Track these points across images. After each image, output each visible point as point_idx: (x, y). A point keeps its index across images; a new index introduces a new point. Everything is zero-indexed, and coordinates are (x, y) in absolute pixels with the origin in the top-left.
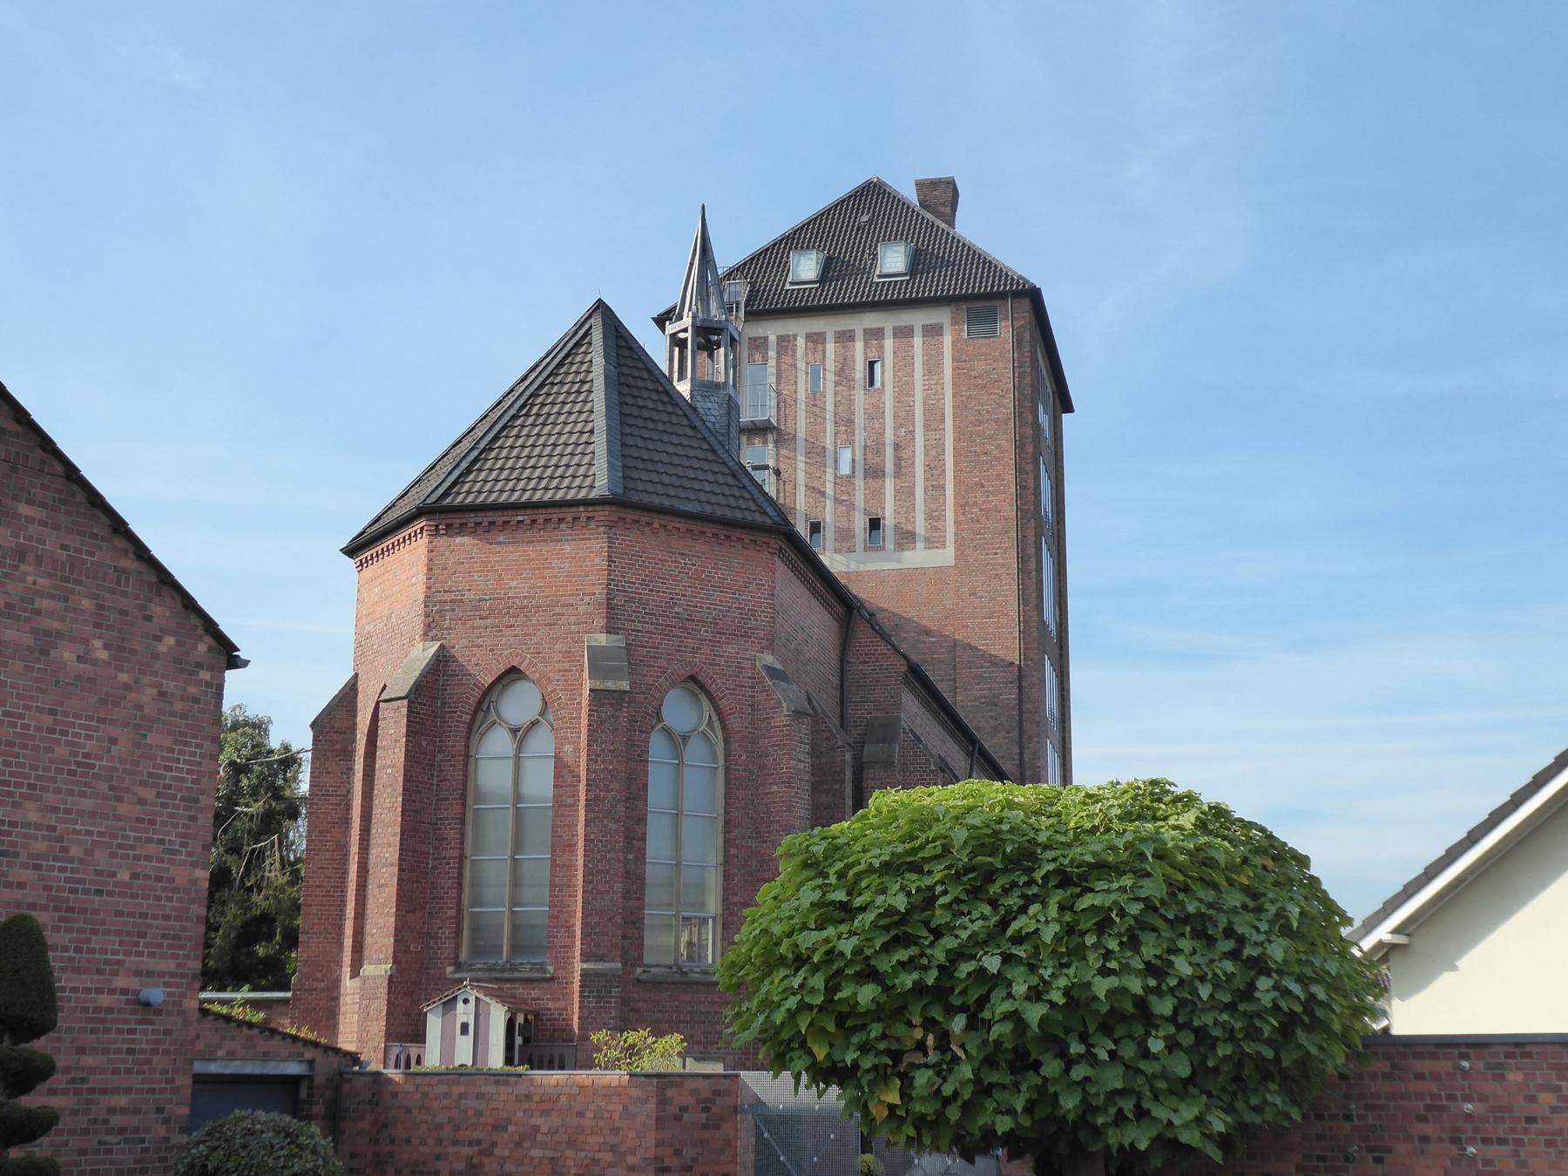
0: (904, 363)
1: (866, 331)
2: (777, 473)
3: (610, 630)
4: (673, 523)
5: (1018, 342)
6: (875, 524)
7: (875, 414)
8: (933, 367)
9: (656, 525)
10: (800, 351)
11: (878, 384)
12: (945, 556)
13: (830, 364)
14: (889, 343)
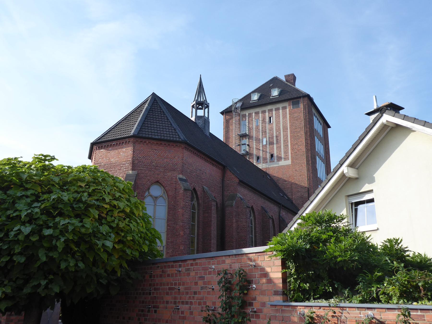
0: (278, 117)
1: (268, 110)
2: (248, 145)
3: (133, 170)
4: (152, 141)
5: (305, 108)
6: (272, 156)
7: (271, 129)
8: (284, 117)
9: (147, 142)
10: (254, 117)
11: (272, 122)
12: (289, 162)
13: (260, 119)
14: (274, 112)
